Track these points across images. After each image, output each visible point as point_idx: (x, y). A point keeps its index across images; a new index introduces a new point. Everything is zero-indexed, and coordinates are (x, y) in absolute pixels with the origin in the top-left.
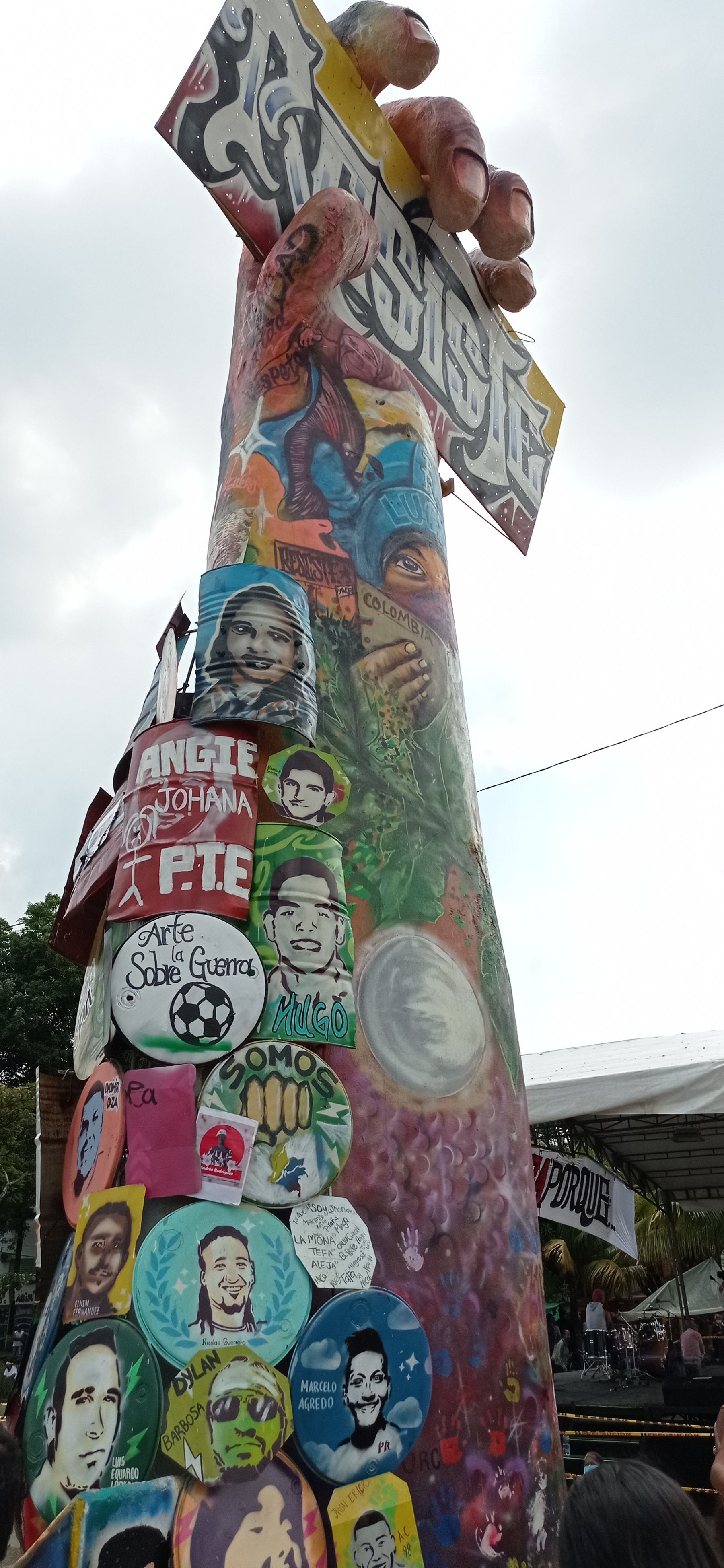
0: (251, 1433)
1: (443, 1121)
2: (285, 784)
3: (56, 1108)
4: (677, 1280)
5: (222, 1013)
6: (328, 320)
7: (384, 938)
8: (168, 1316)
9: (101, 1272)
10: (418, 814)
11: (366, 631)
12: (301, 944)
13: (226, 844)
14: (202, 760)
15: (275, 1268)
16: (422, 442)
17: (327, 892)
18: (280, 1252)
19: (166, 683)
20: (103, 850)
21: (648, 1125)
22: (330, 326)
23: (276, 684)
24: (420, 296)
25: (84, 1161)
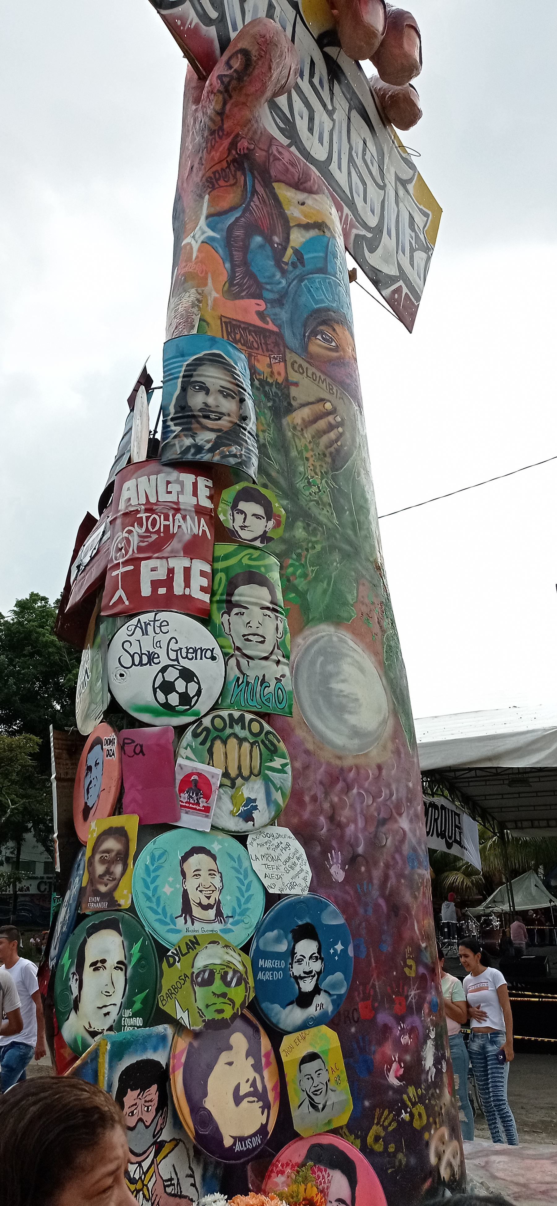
0: (224, 995)
1: (358, 773)
2: (235, 513)
3: (65, 755)
4: (507, 886)
5: (192, 688)
6: (259, 132)
7: (312, 634)
8: (160, 910)
9: (107, 877)
10: (336, 539)
11: (294, 391)
12: (250, 637)
13: (191, 559)
14: (171, 492)
15: (238, 878)
16: (334, 237)
17: (269, 598)
18: (241, 867)
19: (139, 430)
20: (94, 561)
21: (489, 774)
22: (260, 138)
23: (226, 432)
24: (330, 114)
25: (89, 795)
